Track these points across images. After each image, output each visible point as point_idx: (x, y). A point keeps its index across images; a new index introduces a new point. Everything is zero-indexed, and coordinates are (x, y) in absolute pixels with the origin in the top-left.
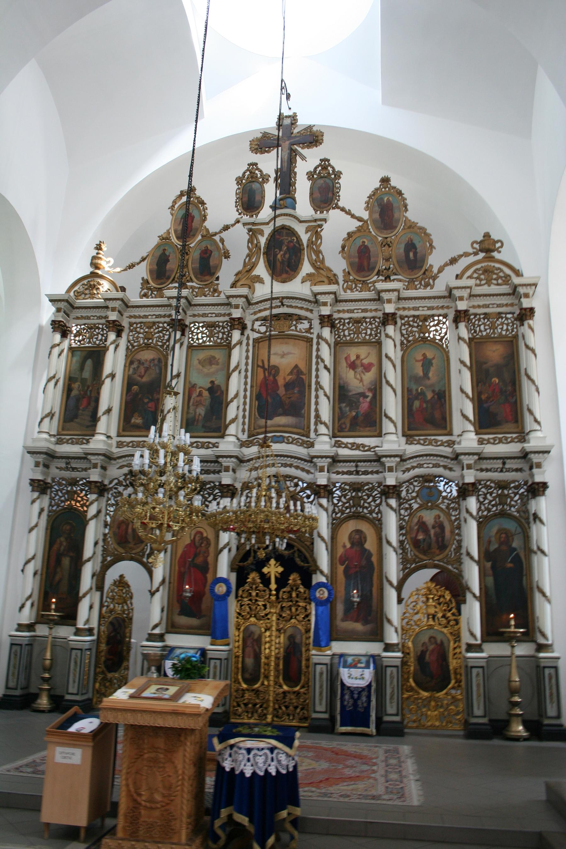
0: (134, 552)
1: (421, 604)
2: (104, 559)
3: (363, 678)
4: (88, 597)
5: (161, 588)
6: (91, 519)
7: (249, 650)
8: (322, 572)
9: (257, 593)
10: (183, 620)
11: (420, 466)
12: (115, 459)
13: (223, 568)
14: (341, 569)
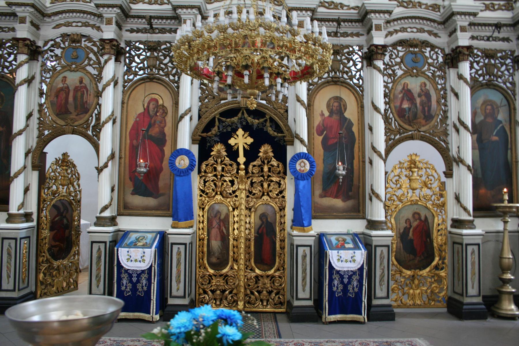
0: (76, 123)
1: (403, 178)
2: (41, 135)
3: (354, 261)
4: (21, 177)
5: (110, 164)
6: (21, 84)
7: (214, 232)
8: (302, 141)
9: (223, 168)
10: (138, 200)
11: (403, 30)
12: (49, 16)
13: (184, 140)
14: (318, 139)
